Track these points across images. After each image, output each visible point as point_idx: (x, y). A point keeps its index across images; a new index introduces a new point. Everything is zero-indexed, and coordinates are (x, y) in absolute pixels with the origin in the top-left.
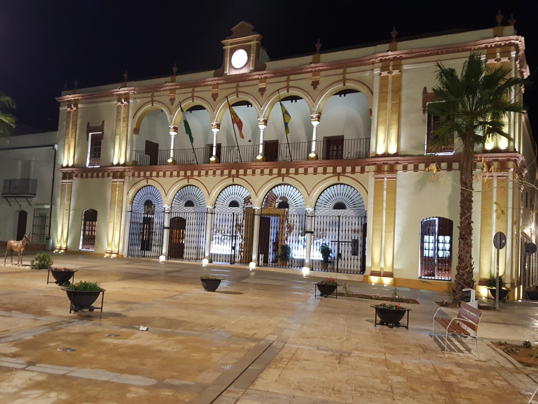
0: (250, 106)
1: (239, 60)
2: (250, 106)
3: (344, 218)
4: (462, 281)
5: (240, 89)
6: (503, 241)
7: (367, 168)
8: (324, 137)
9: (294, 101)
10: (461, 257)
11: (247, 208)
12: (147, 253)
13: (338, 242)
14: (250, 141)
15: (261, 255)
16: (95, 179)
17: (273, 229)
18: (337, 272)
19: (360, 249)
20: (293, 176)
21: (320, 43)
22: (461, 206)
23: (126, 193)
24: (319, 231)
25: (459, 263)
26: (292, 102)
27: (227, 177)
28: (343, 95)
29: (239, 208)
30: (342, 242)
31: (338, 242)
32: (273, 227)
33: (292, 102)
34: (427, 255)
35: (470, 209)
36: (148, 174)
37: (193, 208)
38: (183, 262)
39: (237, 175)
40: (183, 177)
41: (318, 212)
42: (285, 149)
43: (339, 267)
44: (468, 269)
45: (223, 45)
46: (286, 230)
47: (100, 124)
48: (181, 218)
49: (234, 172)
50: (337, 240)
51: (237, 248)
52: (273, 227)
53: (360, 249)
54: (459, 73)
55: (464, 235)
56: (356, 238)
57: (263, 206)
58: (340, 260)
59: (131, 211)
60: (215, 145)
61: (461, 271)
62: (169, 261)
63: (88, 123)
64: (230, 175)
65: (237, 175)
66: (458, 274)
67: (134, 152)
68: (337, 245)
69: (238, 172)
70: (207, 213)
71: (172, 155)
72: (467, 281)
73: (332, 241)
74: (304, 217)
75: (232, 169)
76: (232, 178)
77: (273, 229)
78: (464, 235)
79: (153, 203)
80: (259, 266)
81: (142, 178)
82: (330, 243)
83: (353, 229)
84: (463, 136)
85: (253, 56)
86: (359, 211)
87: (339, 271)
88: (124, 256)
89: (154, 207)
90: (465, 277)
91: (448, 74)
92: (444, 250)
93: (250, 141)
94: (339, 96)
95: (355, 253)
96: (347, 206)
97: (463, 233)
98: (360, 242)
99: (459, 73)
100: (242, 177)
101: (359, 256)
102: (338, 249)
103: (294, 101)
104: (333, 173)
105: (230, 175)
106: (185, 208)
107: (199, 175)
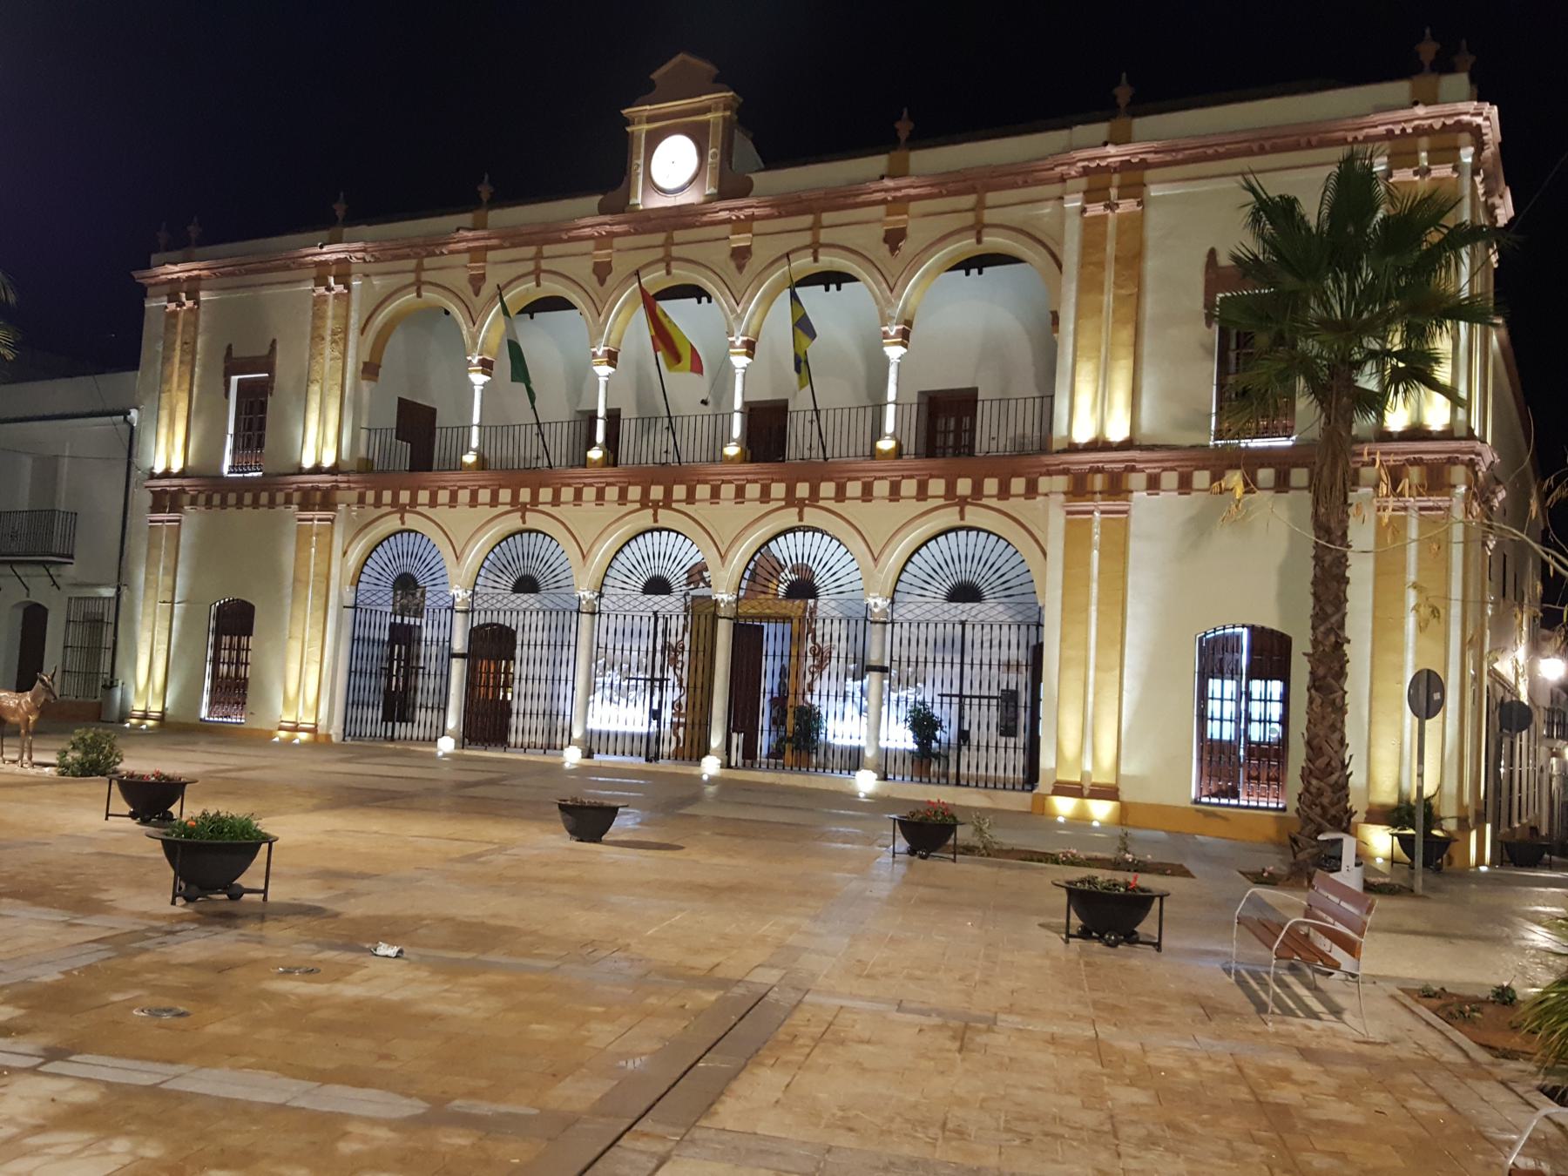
0: (704, 299)
1: (674, 165)
2: (704, 299)
3: (978, 627)
4: (1318, 810)
5: (675, 251)
6: (1437, 696)
7: (1044, 483)
8: (921, 393)
9: (833, 287)
10: (1315, 742)
11: (694, 598)
12: (402, 730)
13: (961, 696)
14: (704, 402)
15: (735, 735)
16: (1263, 497)
17: (770, 659)
18: (958, 784)
19: (1023, 718)
20: (994, 503)
21: (1434, 37)
22: (1315, 594)
23: (340, 554)
24: (904, 664)
25: (1309, 759)
26: (827, 289)
27: (638, 505)
28: (974, 272)
29: (672, 599)
30: (971, 697)
31: (961, 696)
32: (771, 653)
33: (827, 289)
34: (1216, 736)
35: (1340, 602)
36: (405, 496)
37: (539, 597)
38: (507, 756)
39: (667, 502)
40: (508, 508)
41: (902, 611)
42: (808, 425)
43: (963, 770)
44: (1334, 777)
45: (628, 122)
46: (810, 661)
47: (265, 352)
48: (502, 627)
49: (657, 492)
50: (956, 691)
51: (667, 714)
52: (771, 653)
53: (1023, 718)
54: (1312, 209)
55: (1325, 677)
56: (1013, 687)
57: (742, 593)
58: (964, 749)
59: (355, 607)
60: (601, 413)
61: (1314, 782)
62: (467, 752)
63: (229, 348)
64: (645, 502)
65: (667, 502)
66: (1307, 790)
67: (364, 434)
68: (955, 708)
69: (668, 493)
70: (578, 611)
71: (475, 443)
72: (1333, 811)
73: (942, 695)
74: (861, 624)
75: (653, 483)
76: (651, 511)
77: (770, 659)
78: (1325, 677)
79: (420, 583)
80: (729, 766)
81: (389, 509)
82: (937, 699)
83: (1004, 658)
84: (1320, 392)
85: (714, 155)
86: (1020, 608)
87: (963, 782)
88: (334, 739)
89: (423, 595)
90: (1325, 801)
91: (1276, 213)
92: (1264, 721)
93: (704, 402)
94: (963, 272)
95: (1008, 730)
96: (986, 593)
97: (1321, 671)
98: (1024, 698)
99: (1312, 209)
100: (683, 507)
101: (1022, 739)
102: (961, 718)
103: (833, 287)
104: (945, 497)
105: (645, 502)
106: (513, 597)
107: (556, 501)
